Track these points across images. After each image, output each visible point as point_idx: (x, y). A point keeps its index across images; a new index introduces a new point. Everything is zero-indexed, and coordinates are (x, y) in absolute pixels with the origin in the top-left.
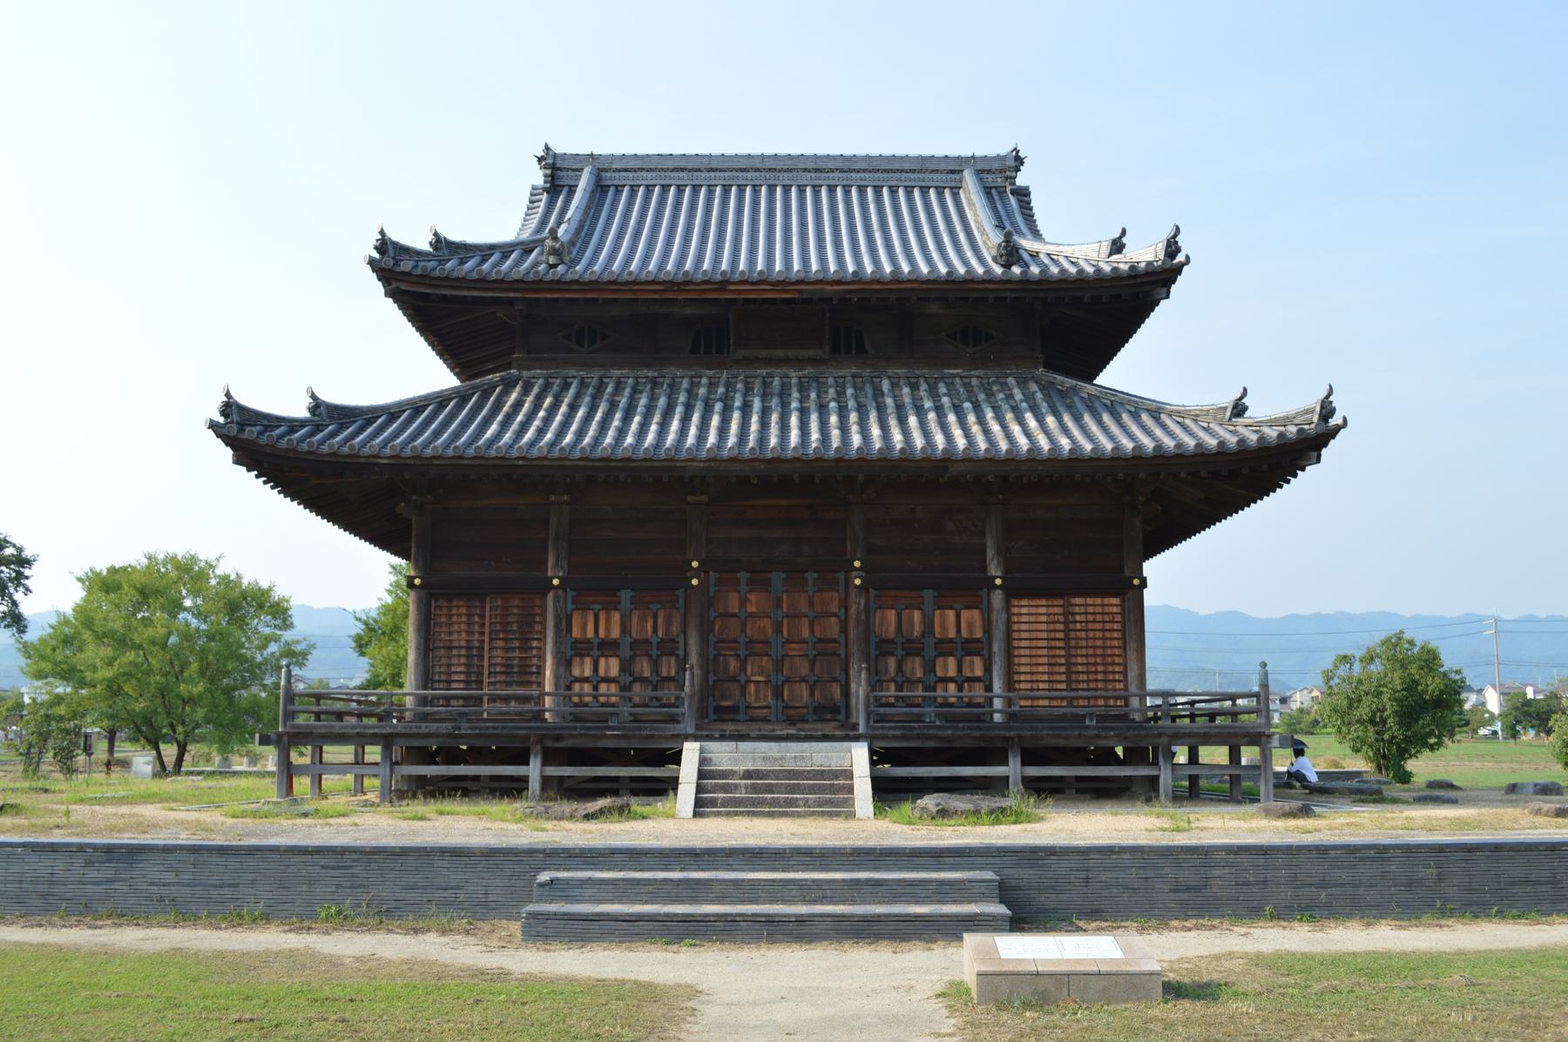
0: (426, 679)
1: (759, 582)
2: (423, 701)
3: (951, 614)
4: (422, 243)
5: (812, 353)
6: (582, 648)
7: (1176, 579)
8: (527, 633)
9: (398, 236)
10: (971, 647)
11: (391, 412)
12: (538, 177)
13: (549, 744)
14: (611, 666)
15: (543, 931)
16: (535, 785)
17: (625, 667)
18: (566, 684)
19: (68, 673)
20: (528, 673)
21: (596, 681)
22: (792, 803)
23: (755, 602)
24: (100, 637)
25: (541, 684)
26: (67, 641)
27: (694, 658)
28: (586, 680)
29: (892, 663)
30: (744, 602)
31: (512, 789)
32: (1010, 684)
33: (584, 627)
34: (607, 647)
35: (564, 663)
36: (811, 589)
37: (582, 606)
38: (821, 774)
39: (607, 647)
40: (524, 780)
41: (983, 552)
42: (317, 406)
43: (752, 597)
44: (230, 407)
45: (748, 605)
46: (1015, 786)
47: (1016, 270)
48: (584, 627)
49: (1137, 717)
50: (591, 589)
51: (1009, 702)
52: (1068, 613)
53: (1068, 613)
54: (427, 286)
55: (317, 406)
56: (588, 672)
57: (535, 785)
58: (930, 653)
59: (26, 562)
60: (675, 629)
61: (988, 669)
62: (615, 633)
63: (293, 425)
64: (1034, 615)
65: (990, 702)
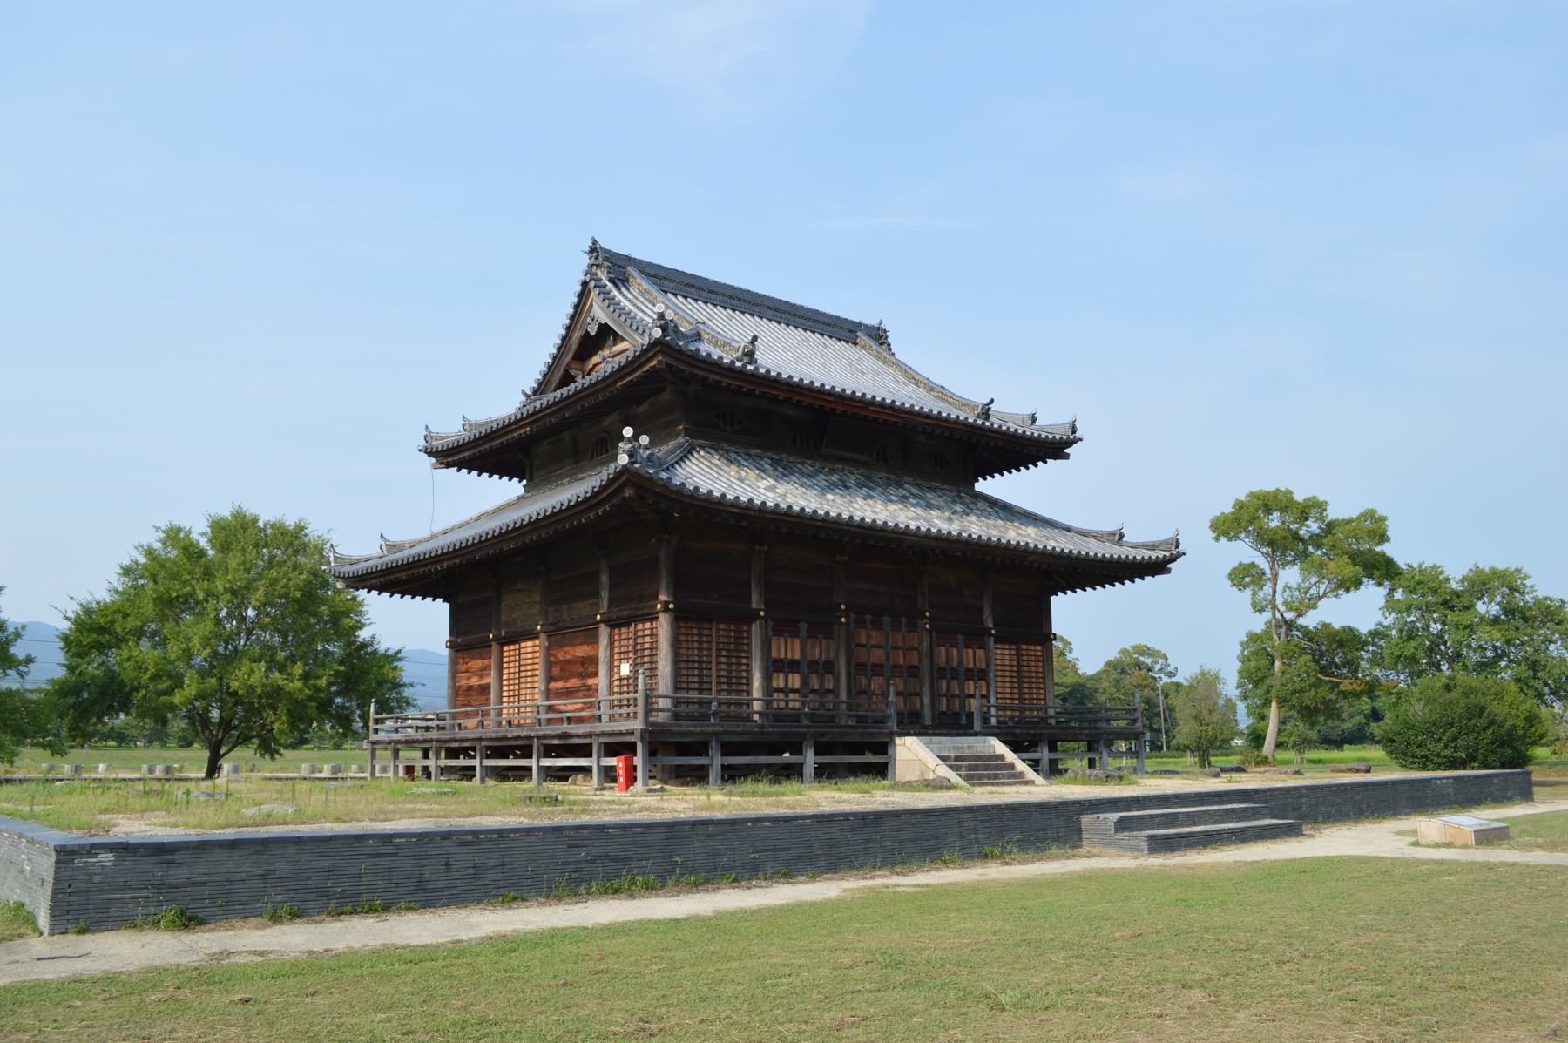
1: (878, 625)
2: (677, 703)
3: (943, 650)
5: (864, 458)
8: (738, 649)
10: (982, 675)
13: (726, 738)
14: (795, 681)
15: (1161, 845)
16: (809, 770)
17: (804, 682)
18: (768, 690)
21: (786, 691)
22: (996, 776)
23: (876, 637)
25: (749, 693)
27: (843, 677)
28: (780, 690)
29: (944, 684)
30: (869, 637)
31: (791, 772)
33: (779, 650)
34: (793, 666)
35: (767, 678)
36: (904, 629)
37: (778, 633)
38: (978, 758)
39: (793, 666)
40: (529, 769)
41: (981, 611)
43: (873, 633)
45: (875, 643)
46: (714, 773)
47: (750, 367)
49: (1053, 722)
50: (782, 626)
51: (768, 703)
52: (1019, 655)
53: (1019, 655)
56: (782, 685)
57: (809, 770)
58: (962, 677)
60: (832, 654)
61: (837, 683)
62: (797, 656)
65: (749, 705)
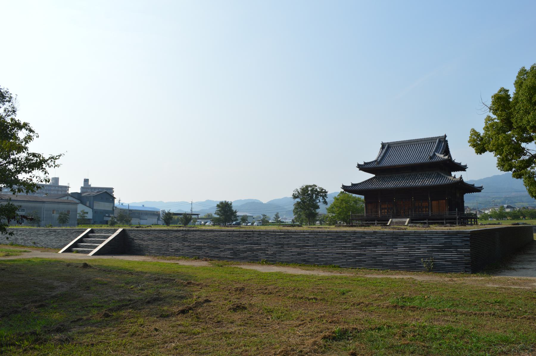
0: (367, 213)
4: (363, 163)
6: (383, 209)
7: (467, 197)
9: (360, 163)
11: (360, 184)
12: (381, 146)
18: (381, 213)
19: (333, 212)
20: (377, 212)
24: (337, 207)
26: (332, 208)
32: (432, 211)
33: (383, 206)
34: (385, 208)
35: (381, 211)
42: (352, 184)
44: (343, 186)
48: (383, 206)
54: (363, 168)
55: (352, 184)
59: (326, 192)
63: (349, 187)
64: (434, 203)
